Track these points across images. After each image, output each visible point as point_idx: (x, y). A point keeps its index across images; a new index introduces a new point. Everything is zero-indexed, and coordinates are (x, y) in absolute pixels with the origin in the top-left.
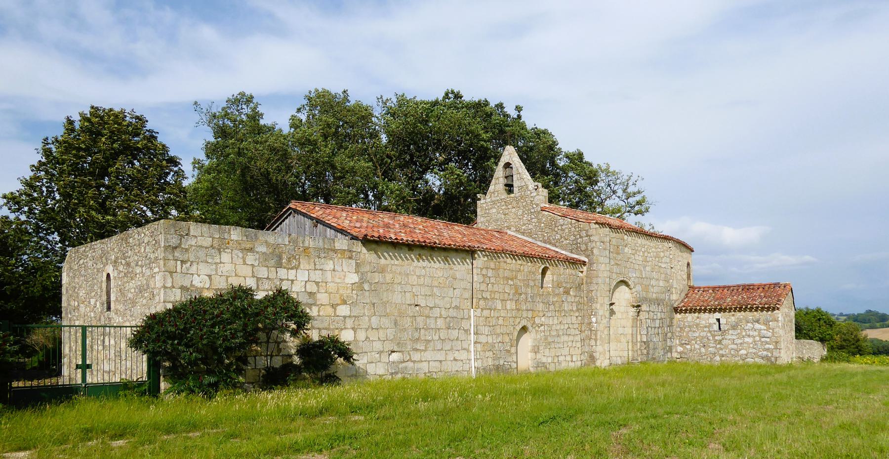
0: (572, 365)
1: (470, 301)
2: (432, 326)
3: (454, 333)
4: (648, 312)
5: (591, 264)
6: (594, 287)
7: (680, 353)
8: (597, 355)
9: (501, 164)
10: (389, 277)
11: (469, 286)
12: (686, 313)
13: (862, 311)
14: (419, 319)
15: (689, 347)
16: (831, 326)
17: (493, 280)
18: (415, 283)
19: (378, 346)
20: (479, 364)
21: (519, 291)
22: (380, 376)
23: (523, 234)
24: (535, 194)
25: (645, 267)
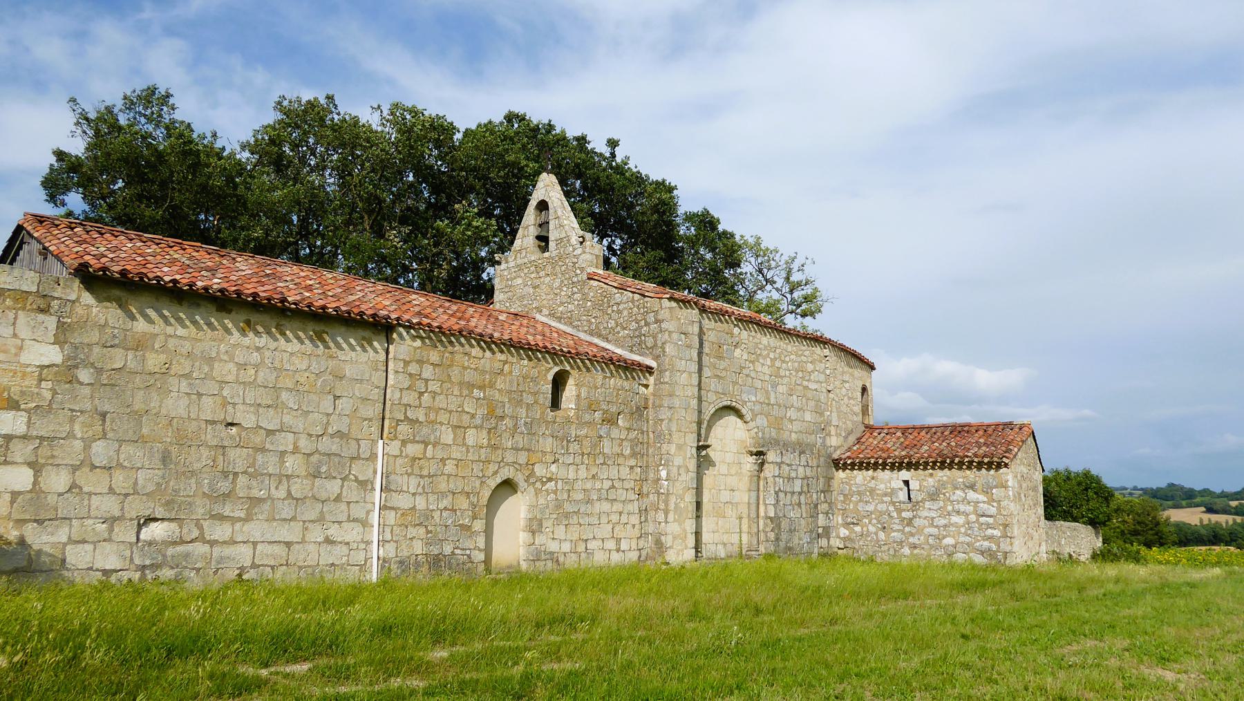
0: (616, 558)
1: (378, 424)
2: (271, 470)
3: (333, 487)
4: (779, 465)
5: (661, 372)
6: (665, 414)
7: (844, 539)
8: (667, 540)
9: (533, 203)
10: (154, 361)
11: (376, 394)
12: (853, 469)
13: (1162, 484)
14: (233, 454)
15: (858, 529)
16: (1106, 499)
17: (434, 386)
18: (230, 378)
19: (110, 505)
20: (390, 551)
21: (499, 412)
22: (106, 572)
23: (559, 319)
24: (579, 251)
25: (775, 386)
